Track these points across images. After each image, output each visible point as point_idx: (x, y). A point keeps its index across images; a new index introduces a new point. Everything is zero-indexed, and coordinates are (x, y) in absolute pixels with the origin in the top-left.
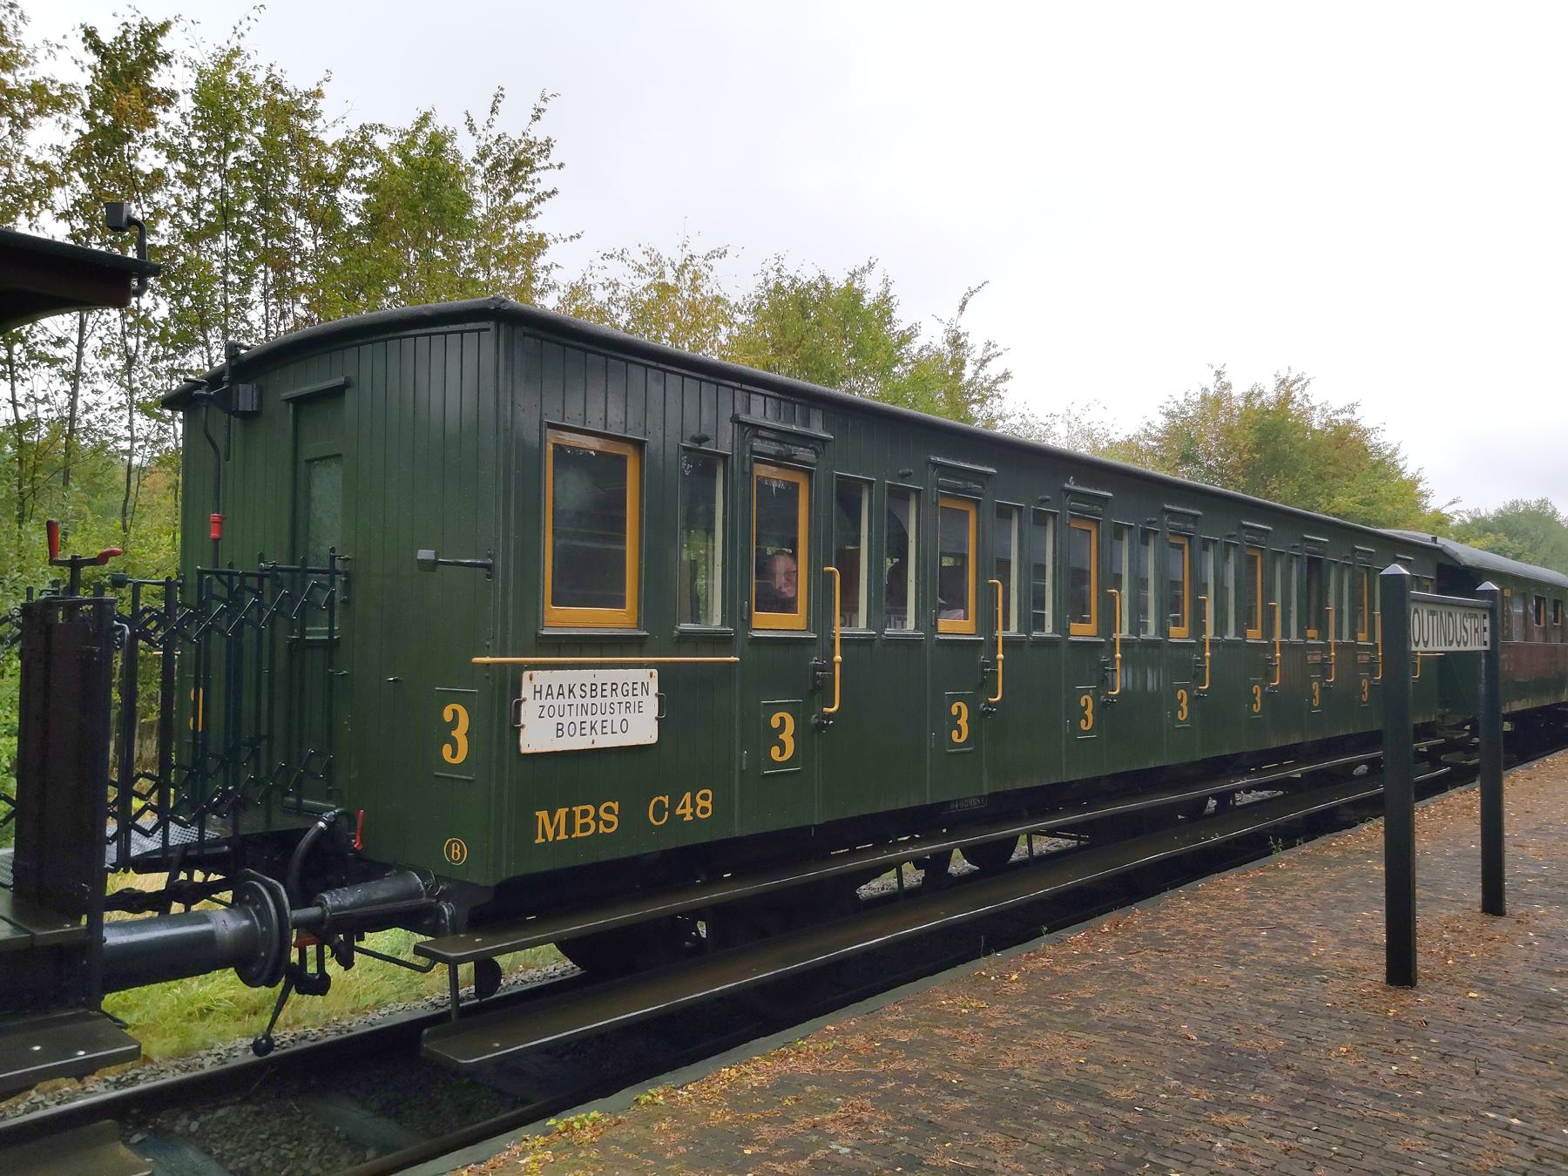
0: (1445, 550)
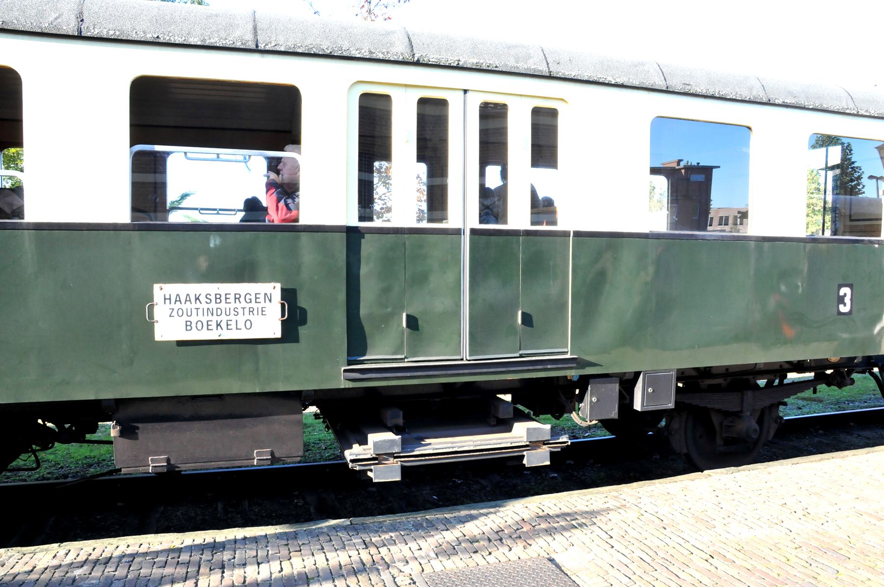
0: (796, 381)
